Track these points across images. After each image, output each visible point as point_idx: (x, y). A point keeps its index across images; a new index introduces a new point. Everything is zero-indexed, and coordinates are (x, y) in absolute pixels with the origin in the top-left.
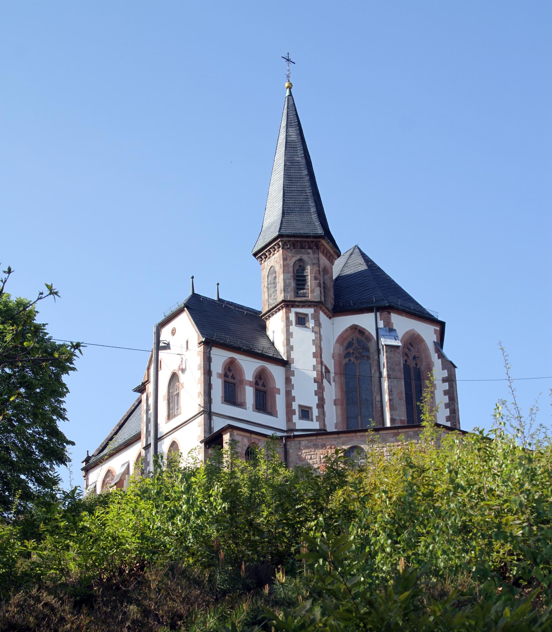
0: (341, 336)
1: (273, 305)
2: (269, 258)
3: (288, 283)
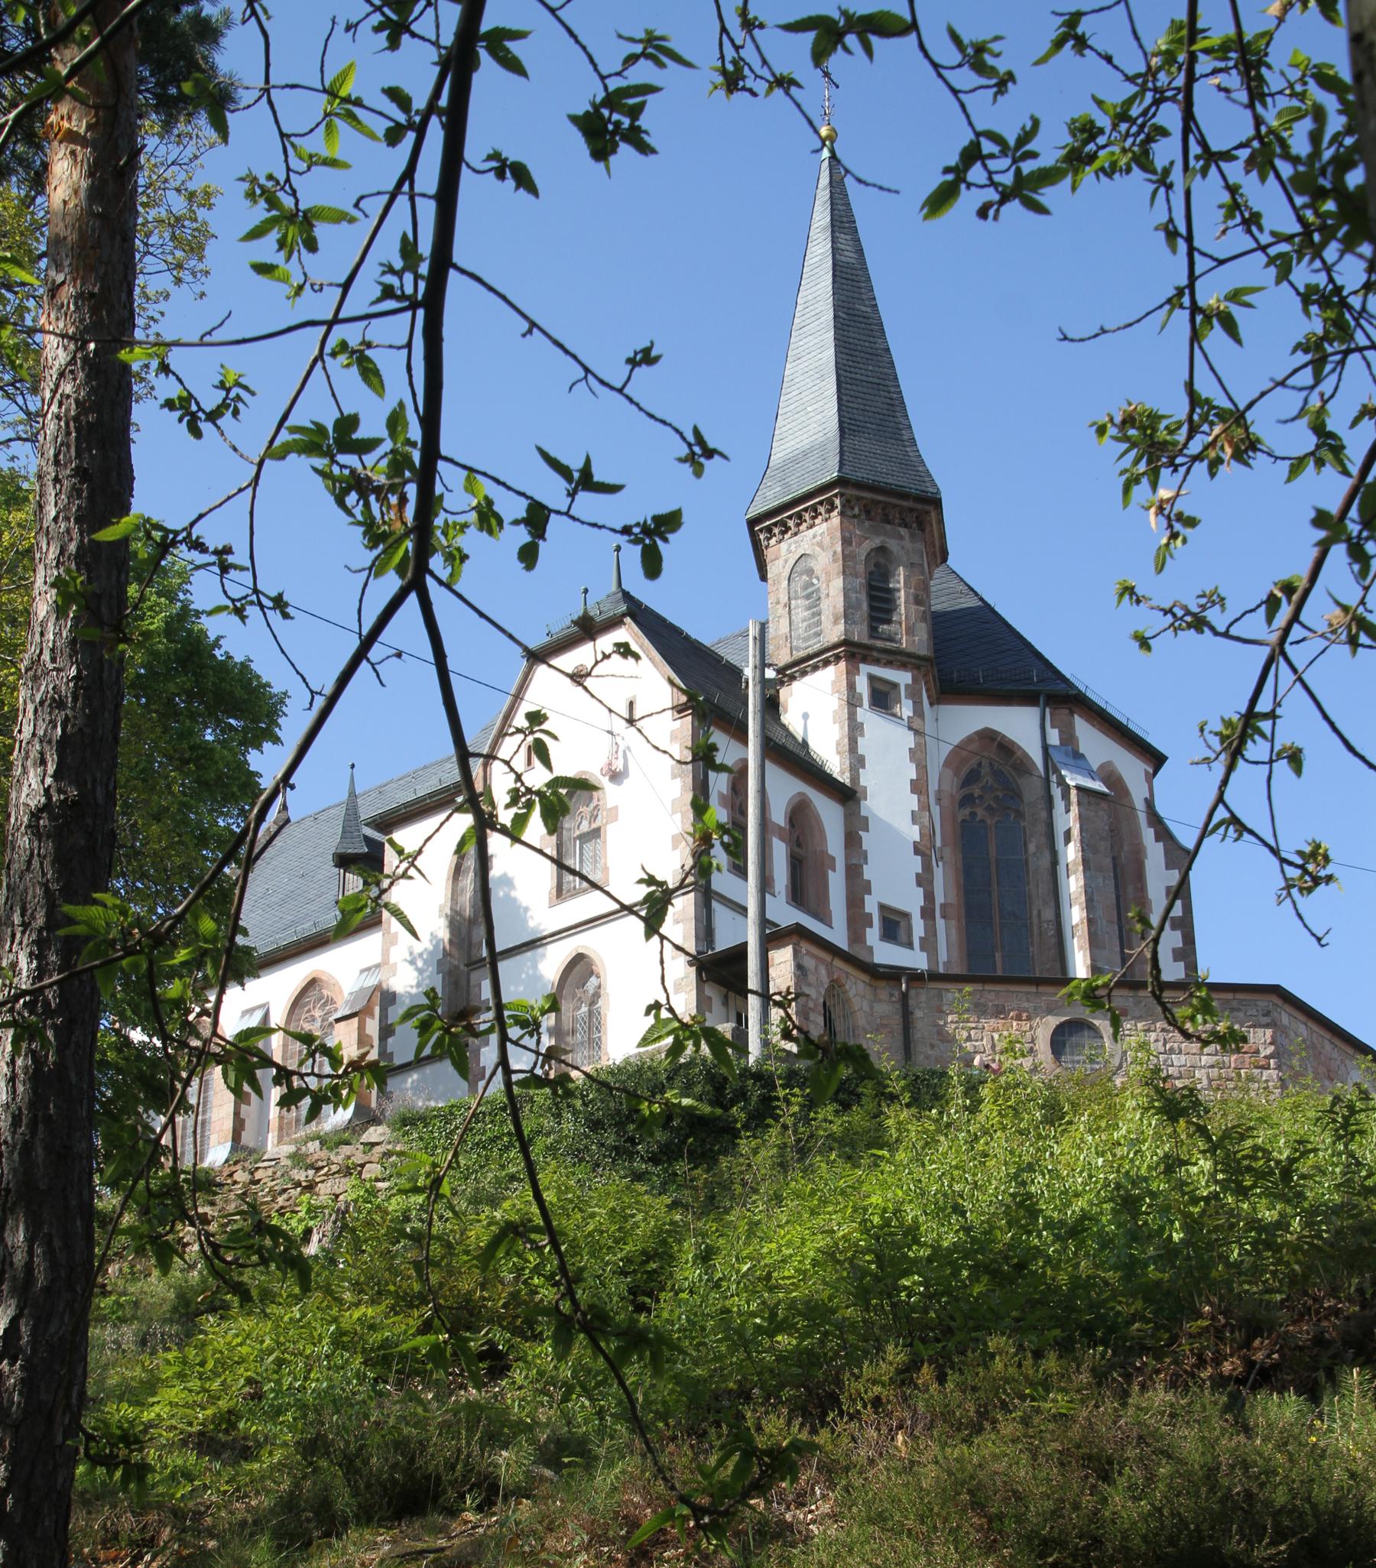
0: (959, 747)
1: (802, 654)
2: (796, 534)
3: (854, 600)
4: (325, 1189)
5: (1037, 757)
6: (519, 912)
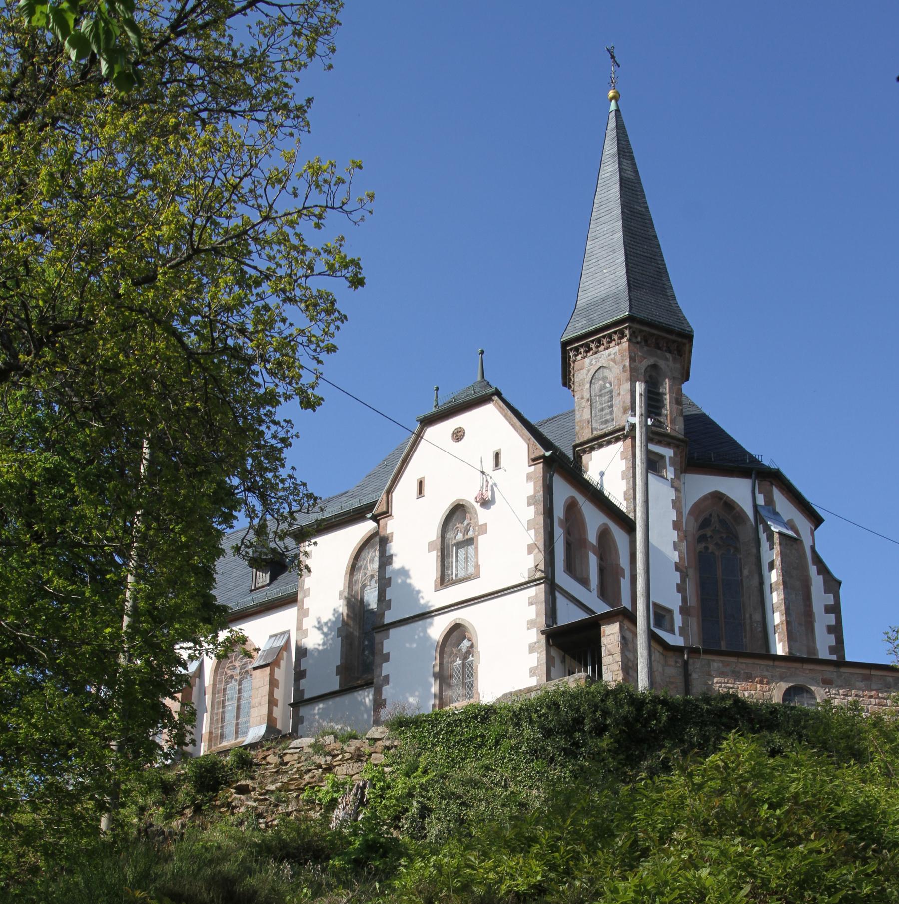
1: (600, 432)
2: (596, 353)
4: (341, 771)
5: (750, 513)
6: (413, 594)
